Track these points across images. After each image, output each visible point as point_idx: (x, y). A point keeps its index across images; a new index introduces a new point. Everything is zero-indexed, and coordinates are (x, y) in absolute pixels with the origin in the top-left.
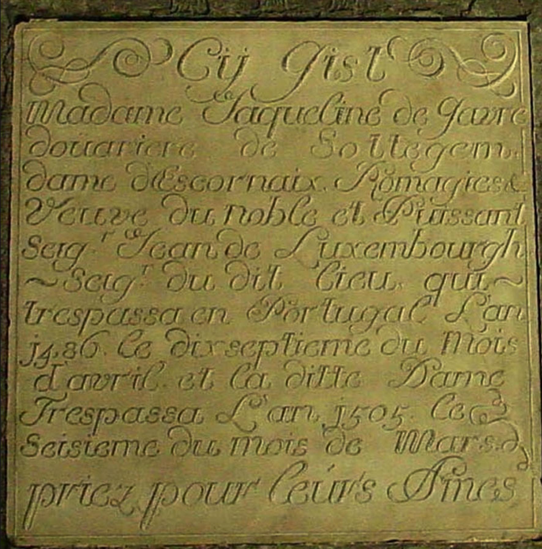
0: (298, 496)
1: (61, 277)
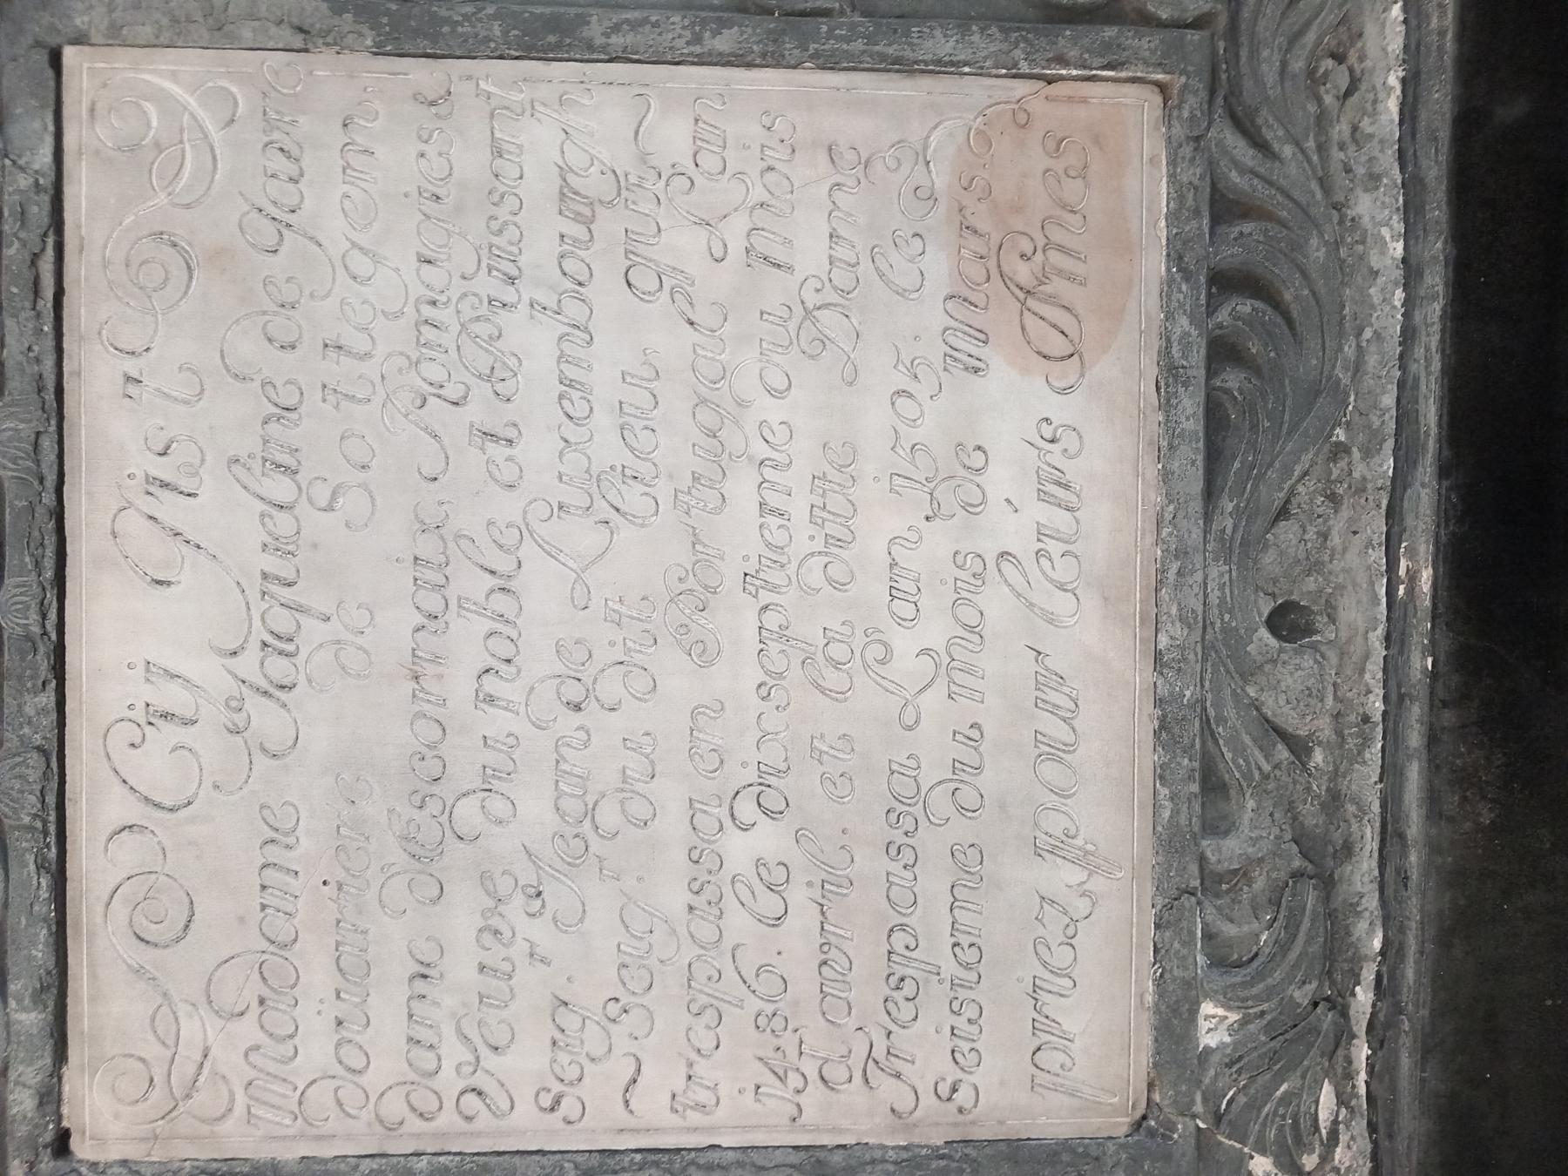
0: (1064, 570)
1: (622, 1044)
